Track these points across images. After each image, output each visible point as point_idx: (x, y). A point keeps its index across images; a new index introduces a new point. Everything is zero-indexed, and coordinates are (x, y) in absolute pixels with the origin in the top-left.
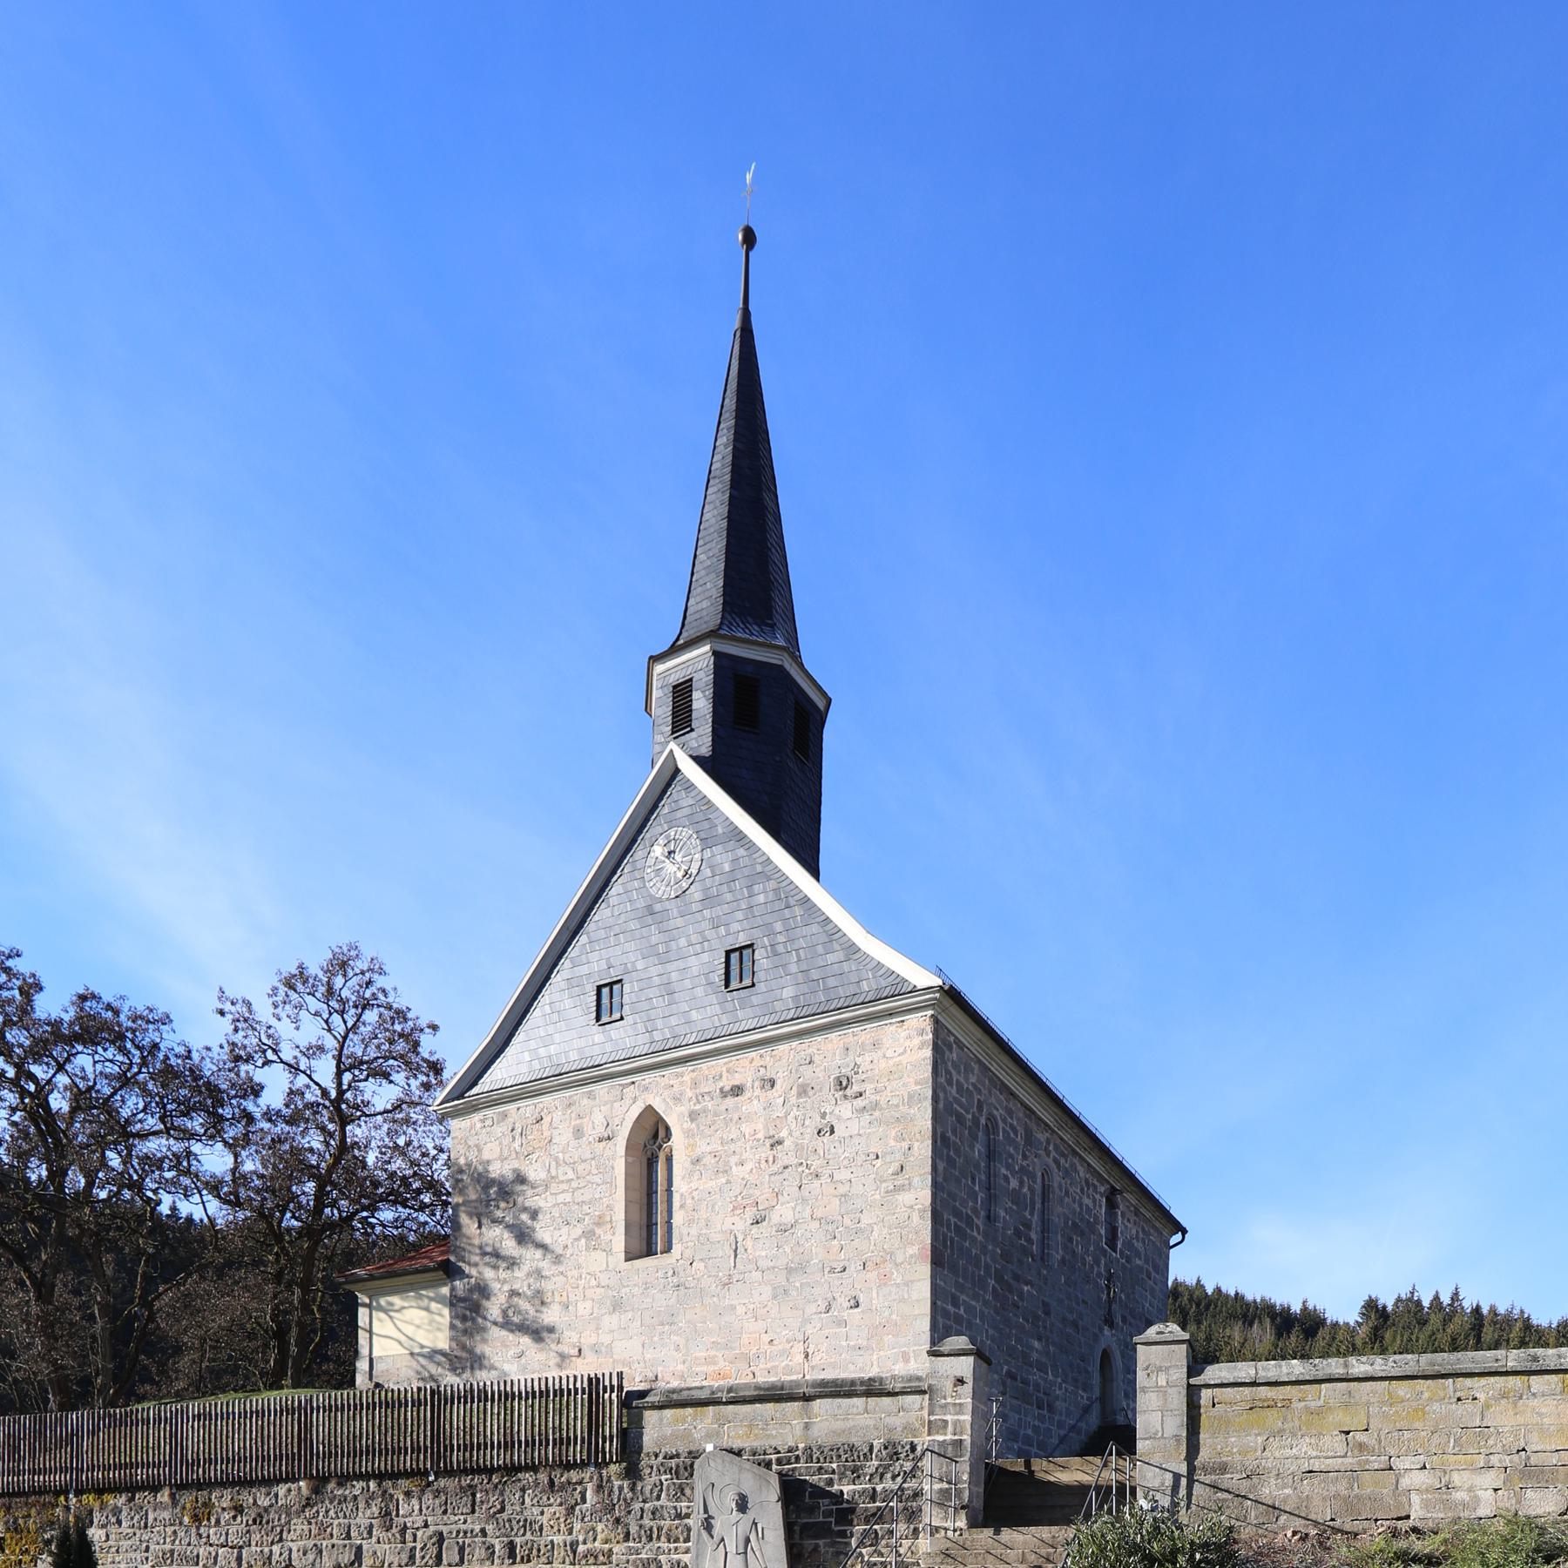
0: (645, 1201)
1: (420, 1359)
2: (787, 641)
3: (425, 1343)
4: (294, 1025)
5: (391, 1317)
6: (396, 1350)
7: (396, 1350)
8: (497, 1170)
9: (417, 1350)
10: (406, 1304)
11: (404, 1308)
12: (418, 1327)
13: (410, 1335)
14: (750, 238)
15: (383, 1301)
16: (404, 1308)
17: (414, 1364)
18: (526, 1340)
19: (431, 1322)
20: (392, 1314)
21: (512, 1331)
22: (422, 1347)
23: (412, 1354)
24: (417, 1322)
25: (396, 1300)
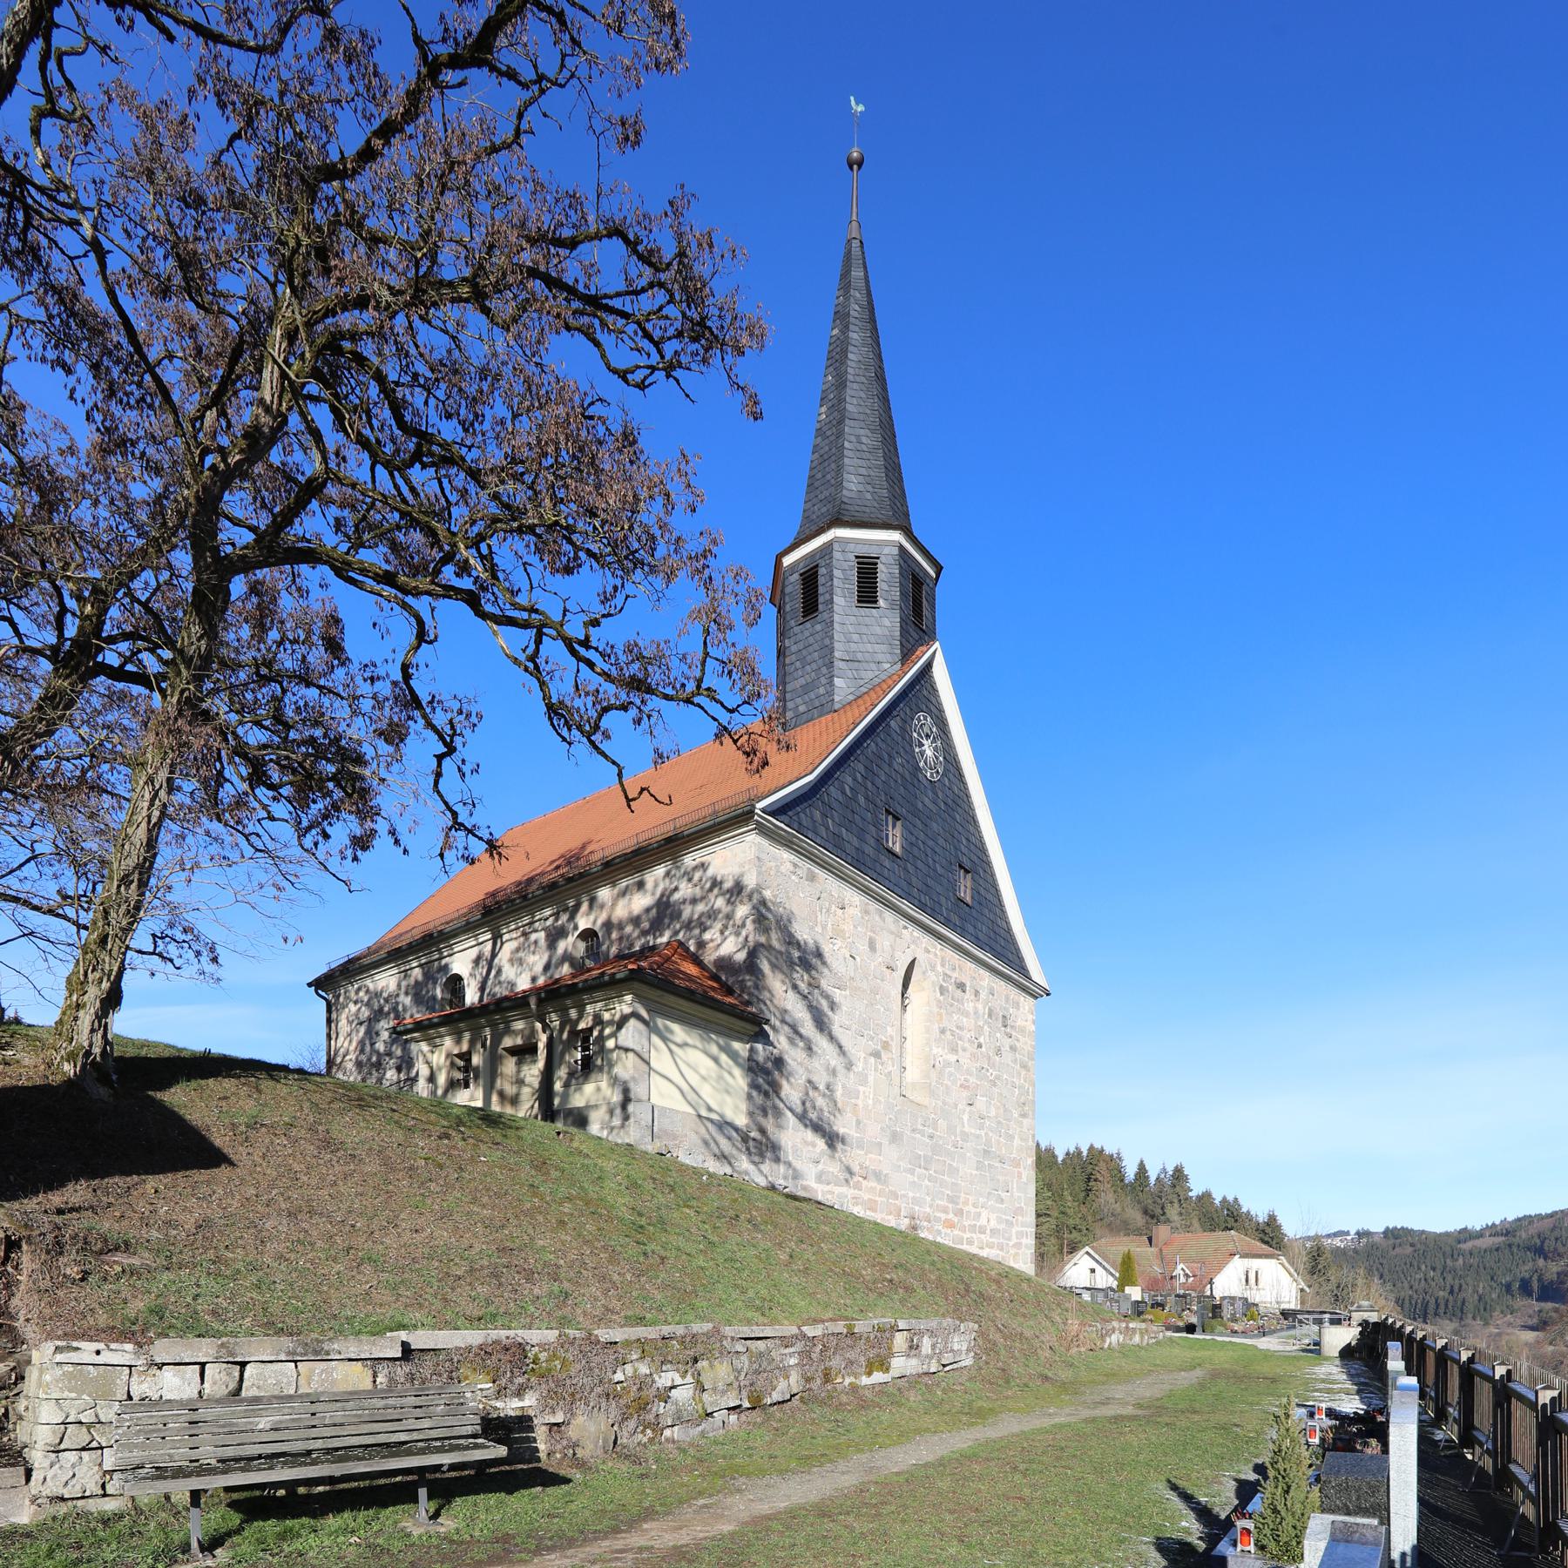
0: (403, 943)
1: (709, 1125)
2: (255, 368)
3: (714, 1106)
4: (715, 550)
5: (671, 1051)
6: (675, 1102)
7: (675, 1102)
8: (802, 932)
9: (704, 1113)
10: (690, 1041)
11: (686, 1044)
12: (704, 1078)
13: (694, 1085)
14: (545, 115)
15: (660, 1022)
16: (686, 1044)
17: (703, 1131)
18: (821, 1144)
19: (720, 1078)
20: (673, 1047)
21: (806, 1126)
22: (710, 1109)
23: (699, 1116)
24: (703, 1072)
25: (679, 1032)
